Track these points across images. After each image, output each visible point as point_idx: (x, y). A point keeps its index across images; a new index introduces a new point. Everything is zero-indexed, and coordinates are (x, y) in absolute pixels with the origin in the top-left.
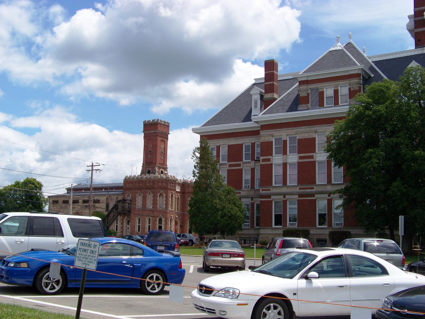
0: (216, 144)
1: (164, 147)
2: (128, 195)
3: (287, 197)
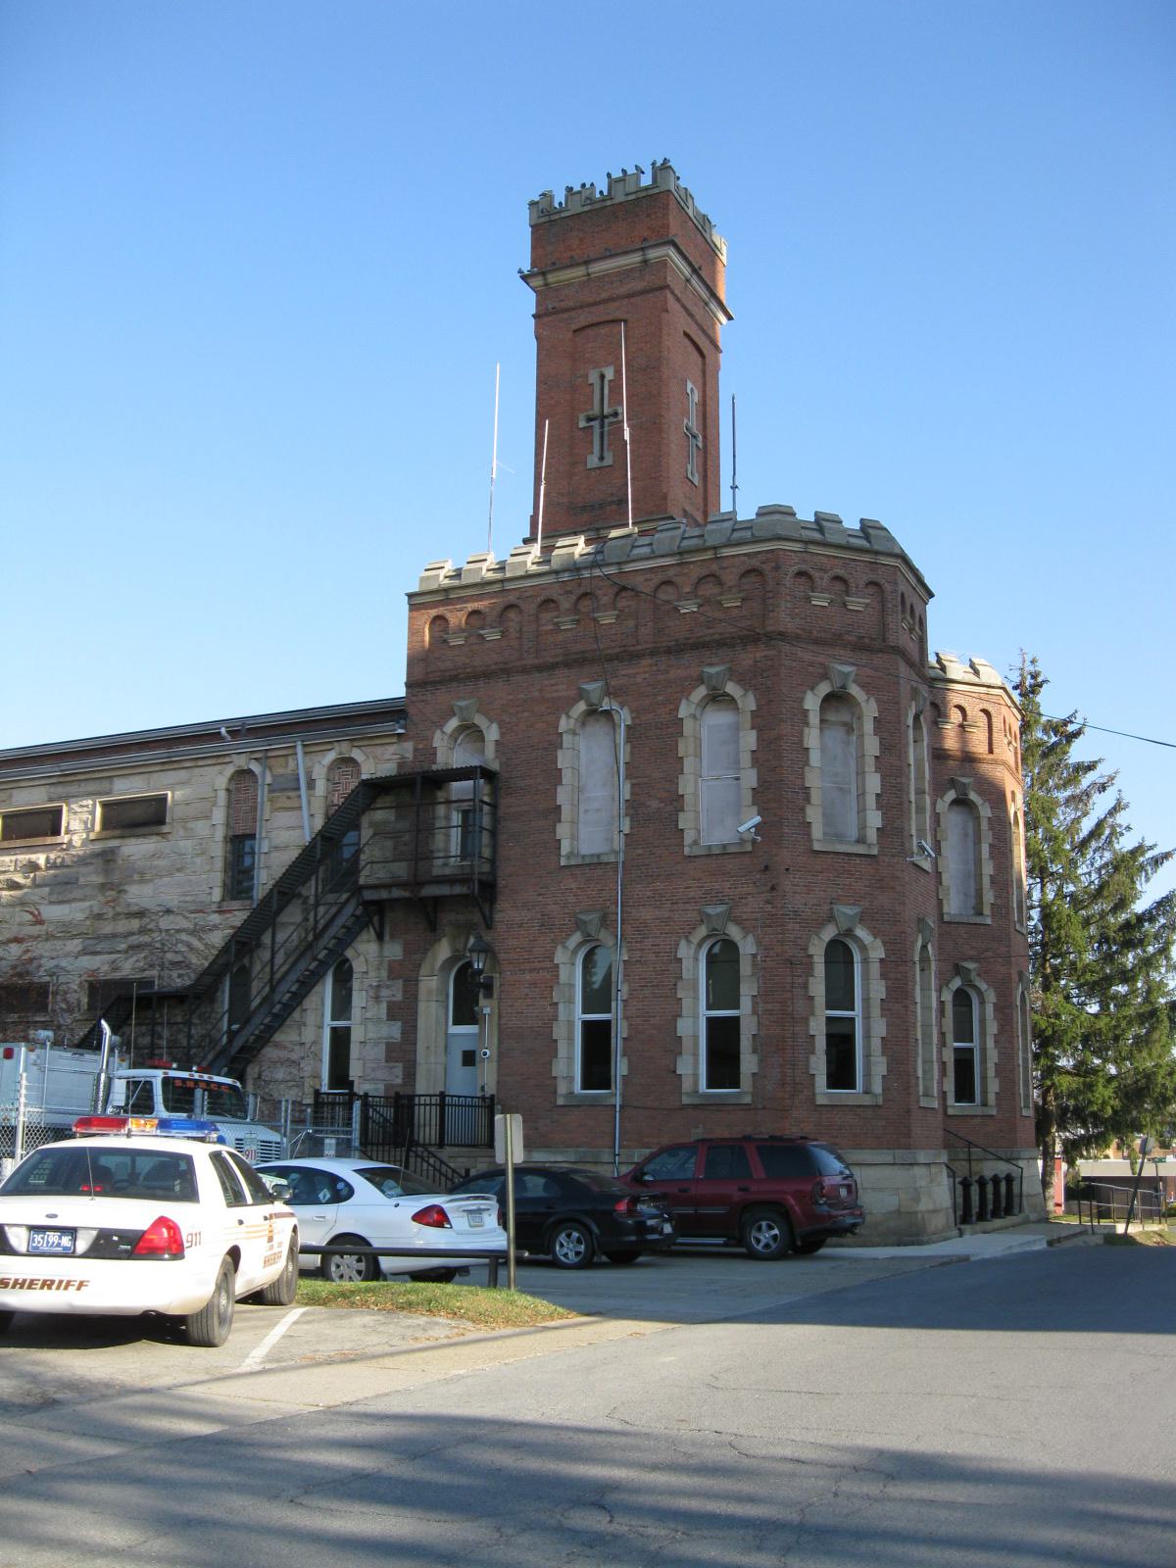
1: (704, 403)
2: (471, 732)
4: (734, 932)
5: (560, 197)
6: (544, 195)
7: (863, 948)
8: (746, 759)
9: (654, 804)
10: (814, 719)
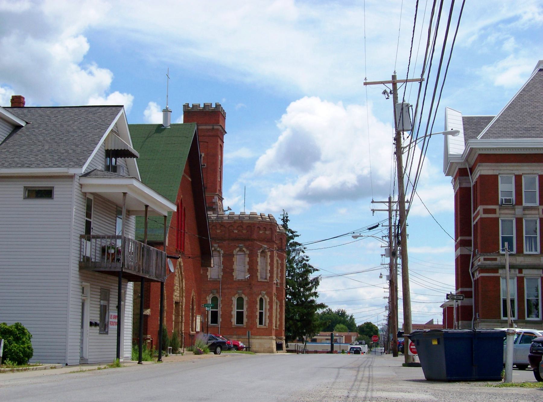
0: (514, 172)
3: (525, 272)
4: (243, 296)
5: (191, 106)
6: (191, 113)
7: (265, 299)
8: (246, 263)
9: (228, 270)
10: (259, 256)
